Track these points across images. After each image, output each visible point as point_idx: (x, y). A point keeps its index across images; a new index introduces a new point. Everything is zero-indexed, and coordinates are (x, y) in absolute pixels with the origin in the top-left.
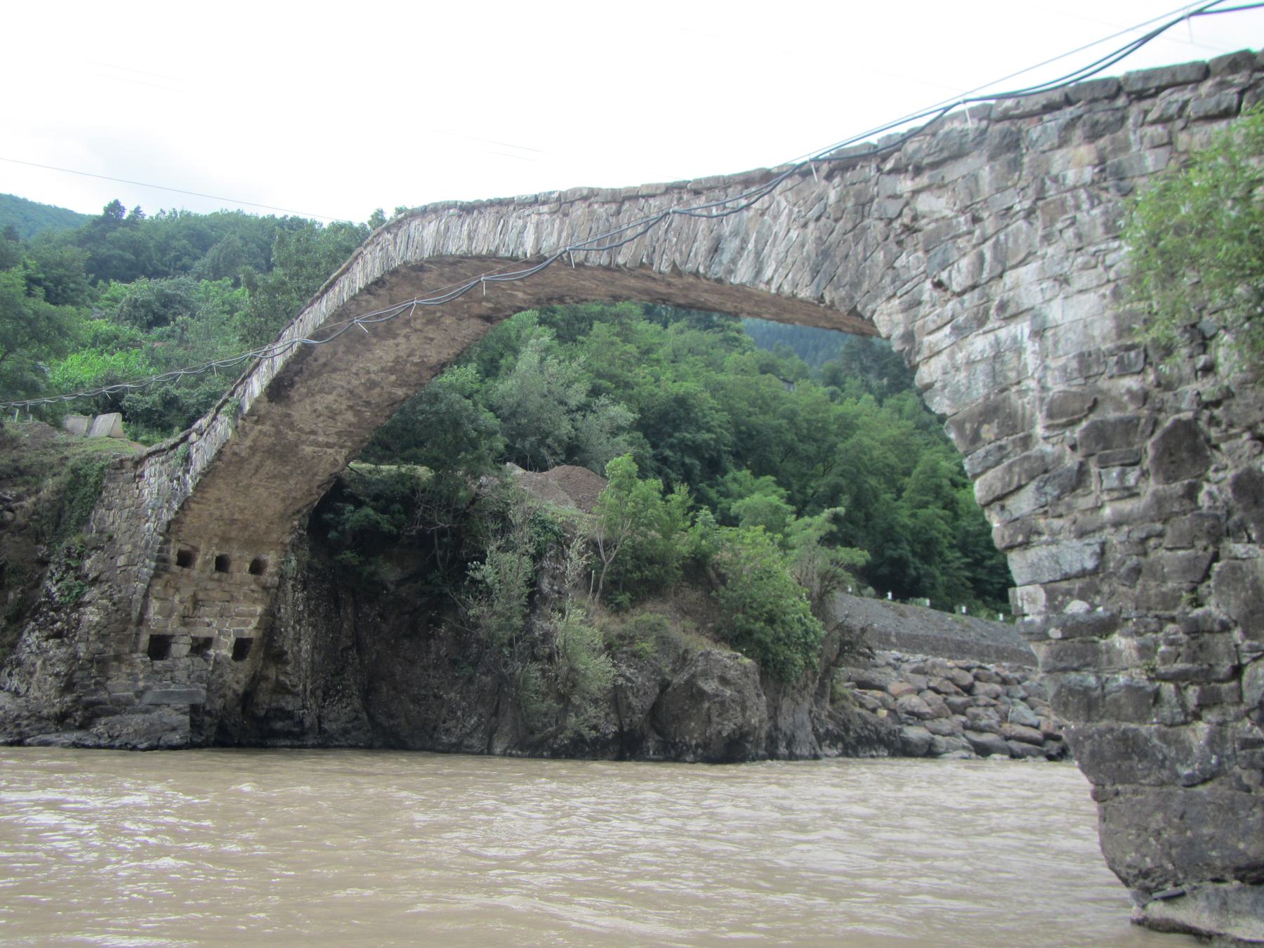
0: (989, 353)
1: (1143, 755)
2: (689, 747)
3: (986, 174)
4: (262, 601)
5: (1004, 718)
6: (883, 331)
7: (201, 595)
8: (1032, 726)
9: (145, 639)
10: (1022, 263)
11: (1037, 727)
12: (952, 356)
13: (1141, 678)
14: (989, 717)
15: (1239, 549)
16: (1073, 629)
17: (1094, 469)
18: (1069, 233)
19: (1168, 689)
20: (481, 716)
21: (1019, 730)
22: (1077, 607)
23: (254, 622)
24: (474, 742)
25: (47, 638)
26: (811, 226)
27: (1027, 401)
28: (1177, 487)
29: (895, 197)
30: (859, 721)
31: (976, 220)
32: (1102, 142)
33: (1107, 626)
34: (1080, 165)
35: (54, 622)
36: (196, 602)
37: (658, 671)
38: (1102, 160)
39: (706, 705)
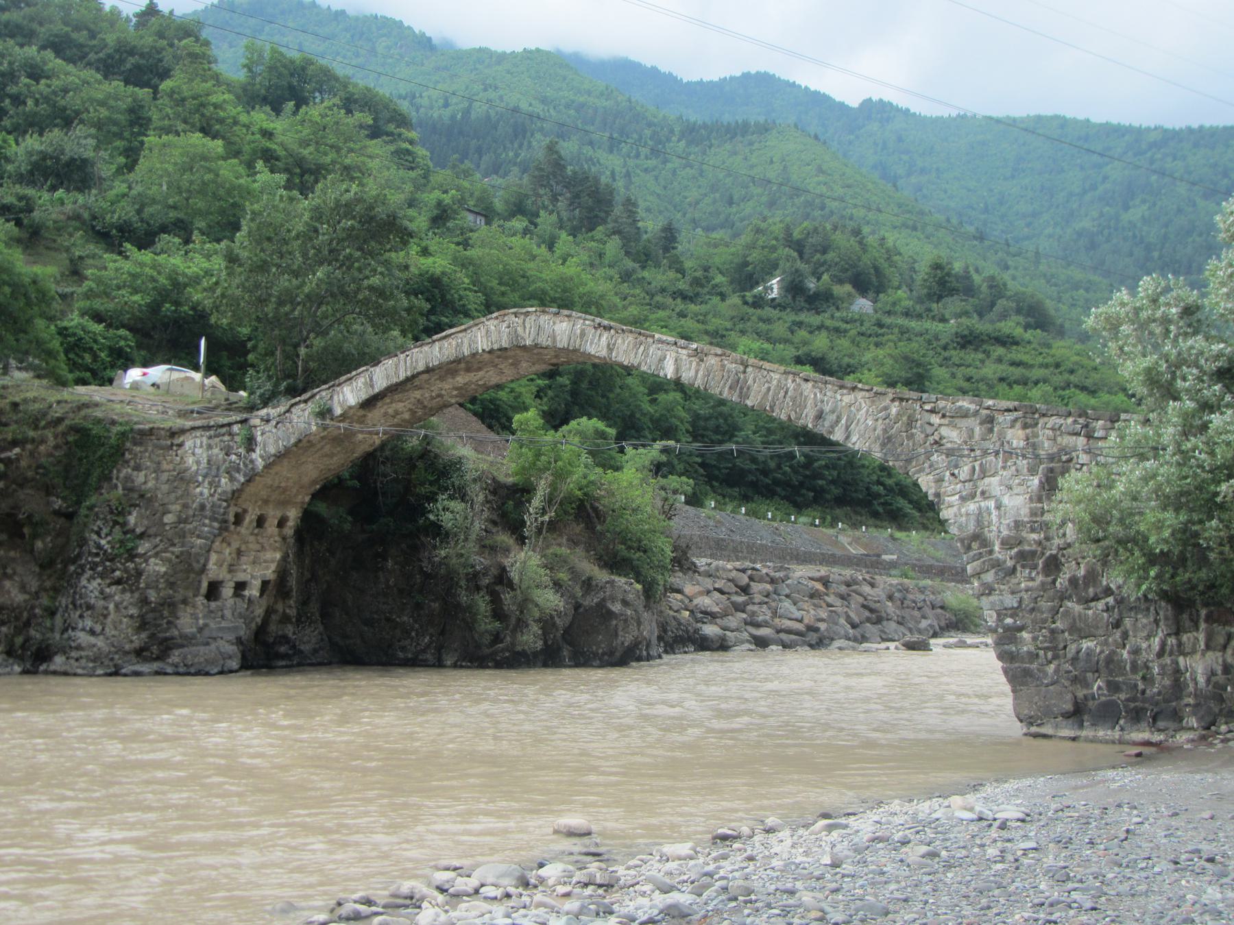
0: (976, 512)
1: (1031, 676)
2: (595, 655)
3: (977, 430)
4: (280, 549)
5: (775, 614)
6: (924, 489)
7: (243, 548)
8: (796, 620)
9: (205, 585)
10: (992, 475)
11: (801, 621)
12: (959, 509)
13: (1032, 648)
14: (764, 614)
15: (1070, 604)
16: (1007, 629)
17: (1019, 568)
18: (1013, 468)
19: (1041, 653)
20: (431, 636)
21: (788, 624)
22: (1009, 621)
23: (273, 567)
24: (429, 656)
25: (109, 585)
26: (880, 421)
27: (991, 534)
28: (1050, 579)
29: (930, 424)
30: (674, 623)
31: (973, 450)
32: (1028, 431)
33: (1021, 629)
34: (1018, 439)
35: (113, 571)
36: (239, 553)
37: (573, 596)
38: (1027, 439)
39: (614, 622)
